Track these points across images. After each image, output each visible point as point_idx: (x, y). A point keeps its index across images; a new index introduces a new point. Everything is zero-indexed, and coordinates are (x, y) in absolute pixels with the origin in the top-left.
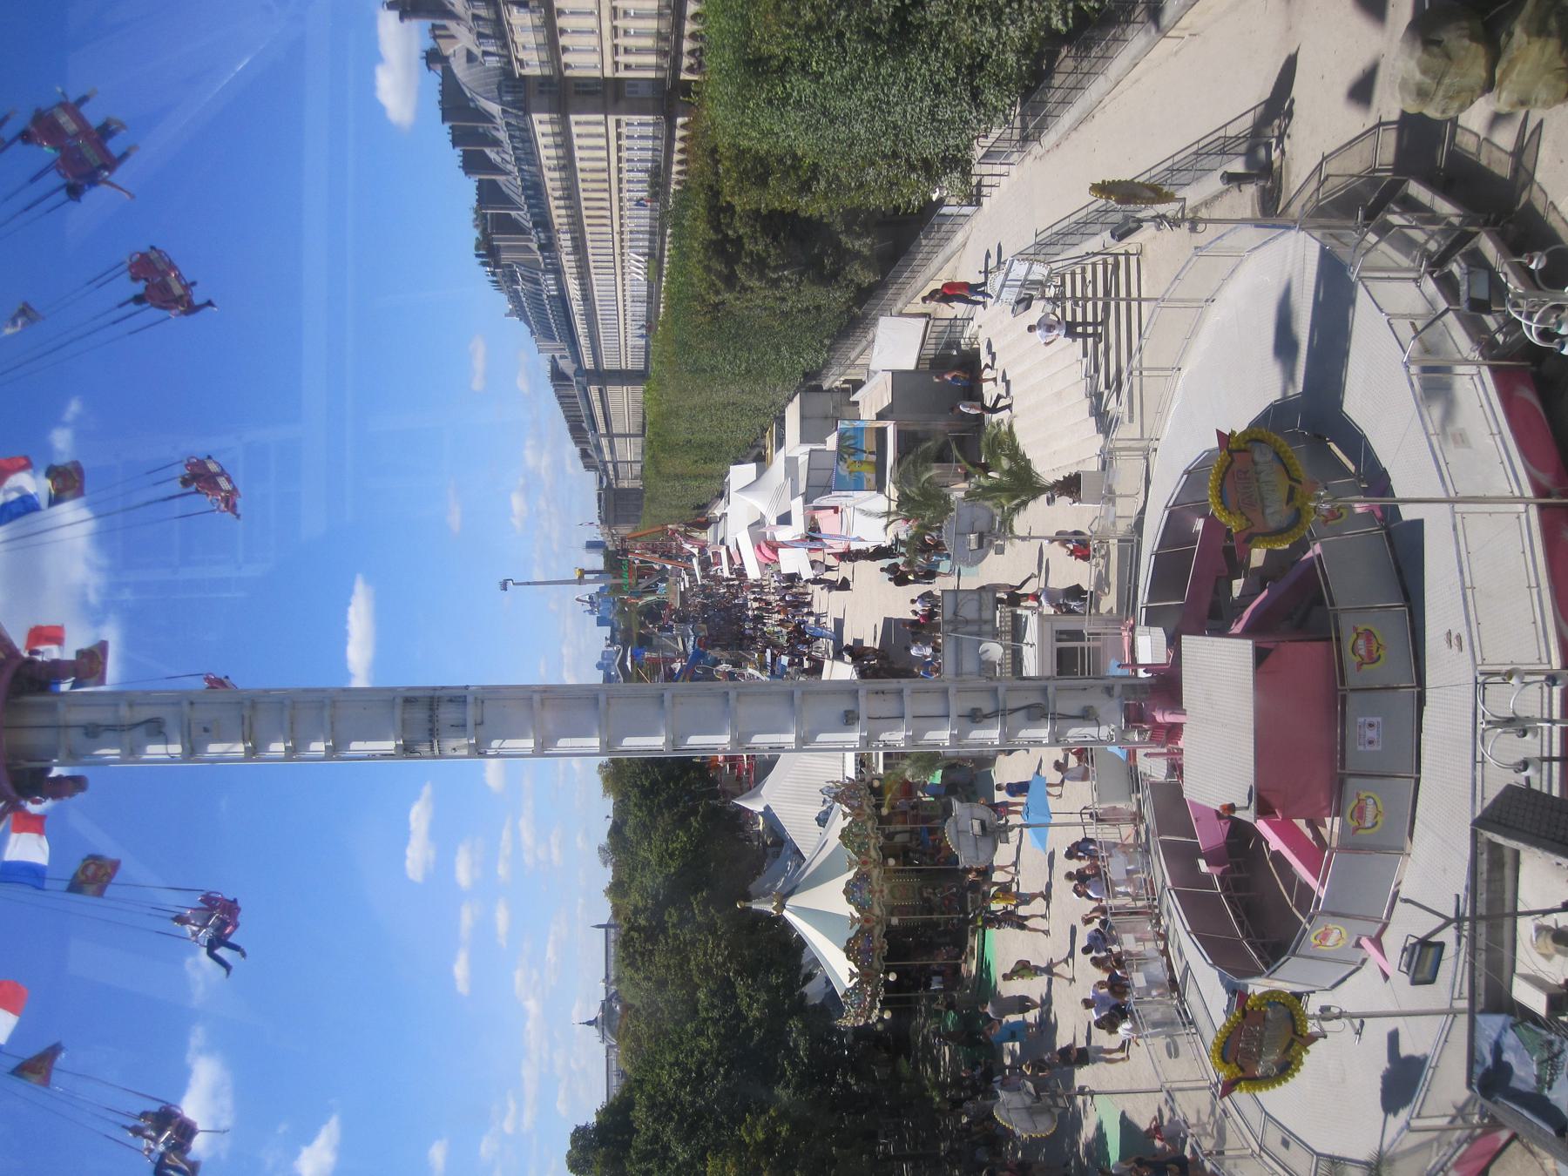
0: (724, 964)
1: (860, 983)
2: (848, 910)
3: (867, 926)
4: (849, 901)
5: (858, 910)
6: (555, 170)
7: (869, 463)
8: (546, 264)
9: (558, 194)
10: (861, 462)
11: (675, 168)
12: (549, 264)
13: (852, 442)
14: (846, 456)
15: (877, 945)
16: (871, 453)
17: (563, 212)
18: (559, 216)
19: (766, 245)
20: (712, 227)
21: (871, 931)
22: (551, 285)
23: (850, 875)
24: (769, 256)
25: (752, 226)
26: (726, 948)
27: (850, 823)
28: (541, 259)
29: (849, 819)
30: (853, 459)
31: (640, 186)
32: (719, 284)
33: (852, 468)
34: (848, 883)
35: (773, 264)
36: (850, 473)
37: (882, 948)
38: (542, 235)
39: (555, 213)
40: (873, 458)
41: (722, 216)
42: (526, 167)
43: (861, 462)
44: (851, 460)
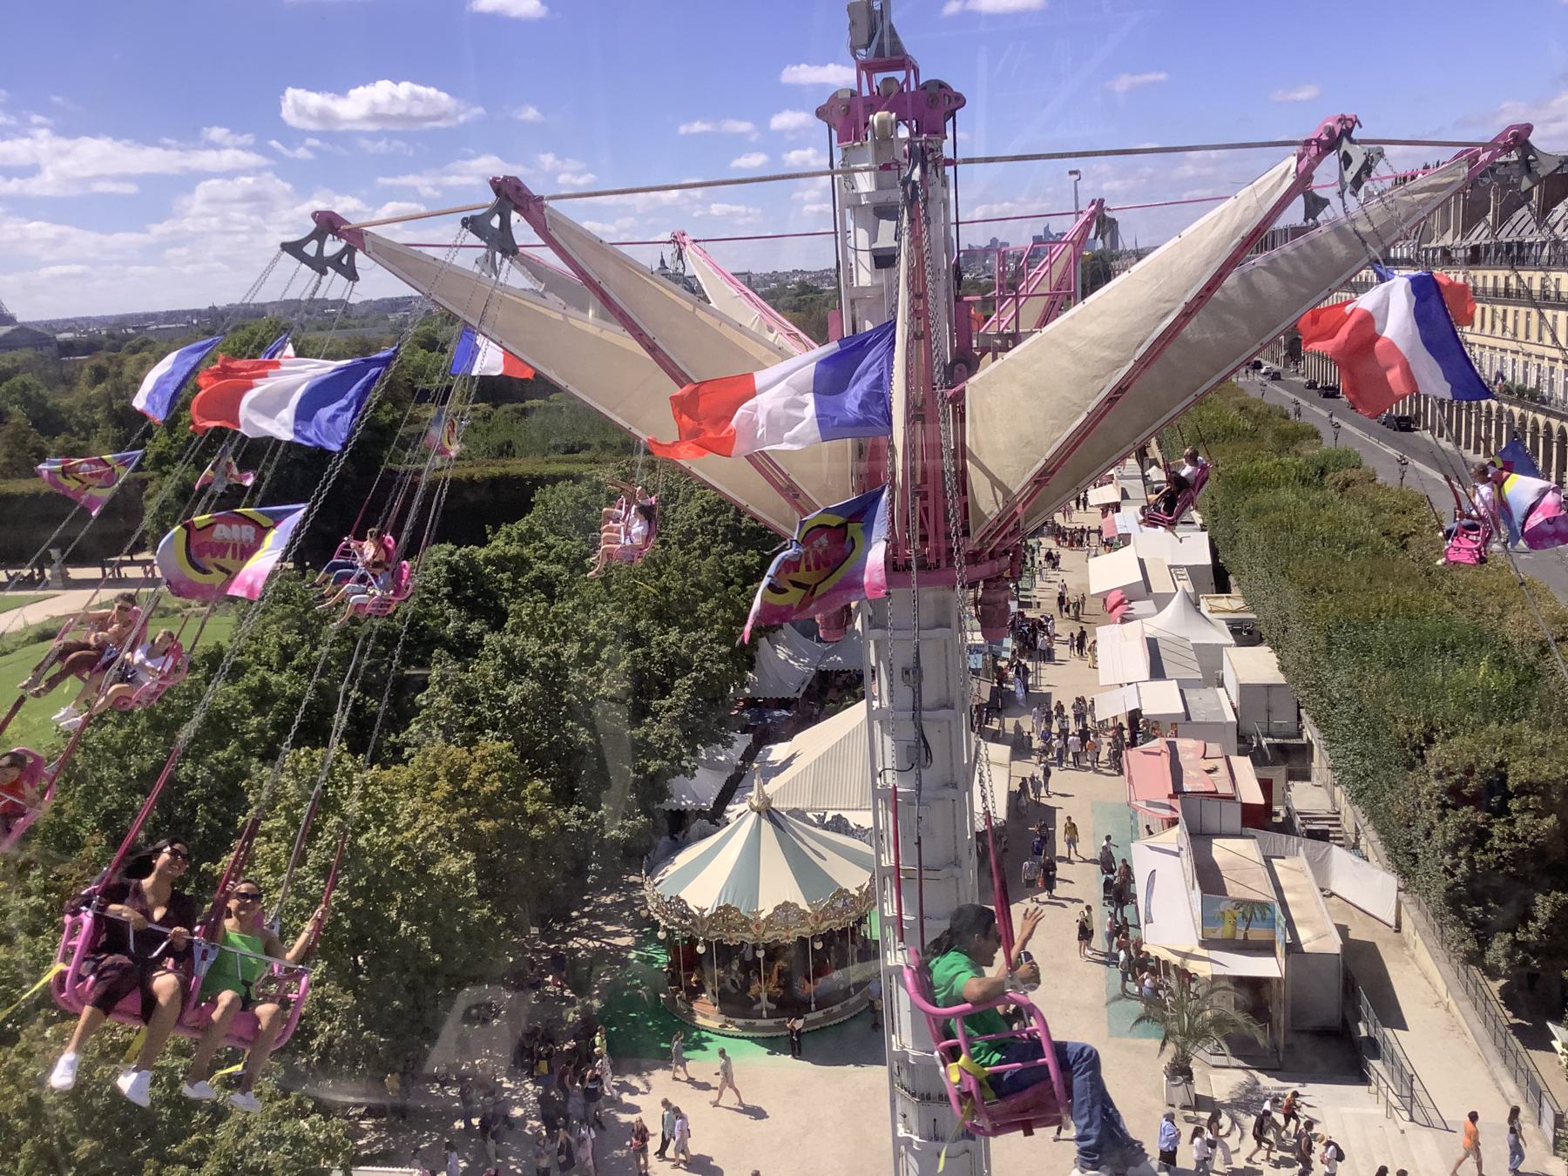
0: (703, 668)
1: (693, 916)
2: (766, 908)
3: (753, 927)
4: (777, 908)
5: (768, 917)
6: (1543, 286)
7: (1234, 933)
8: (1427, 250)
9: (1513, 281)
10: (1235, 925)
11: (1541, 419)
12: (1427, 254)
13: (1259, 916)
14: (1241, 909)
15: (733, 935)
16: (1246, 934)
17: (1490, 284)
18: (1485, 277)
19: (1500, 850)
20: (1522, 785)
21: (748, 930)
22: (1402, 252)
23: (803, 905)
24: (1485, 853)
25: (1524, 838)
26: (719, 670)
27: (853, 896)
28: (1433, 244)
29: (857, 893)
30: (1239, 916)
31: (1519, 374)
32: (1449, 781)
33: (1228, 915)
34: (795, 905)
35: (1476, 858)
36: (1223, 913)
37: (731, 940)
38: (1461, 254)
39: (1490, 274)
40: (1240, 936)
41: (1539, 799)
42: (1546, 251)
43: (1235, 925)
44: (1238, 914)
